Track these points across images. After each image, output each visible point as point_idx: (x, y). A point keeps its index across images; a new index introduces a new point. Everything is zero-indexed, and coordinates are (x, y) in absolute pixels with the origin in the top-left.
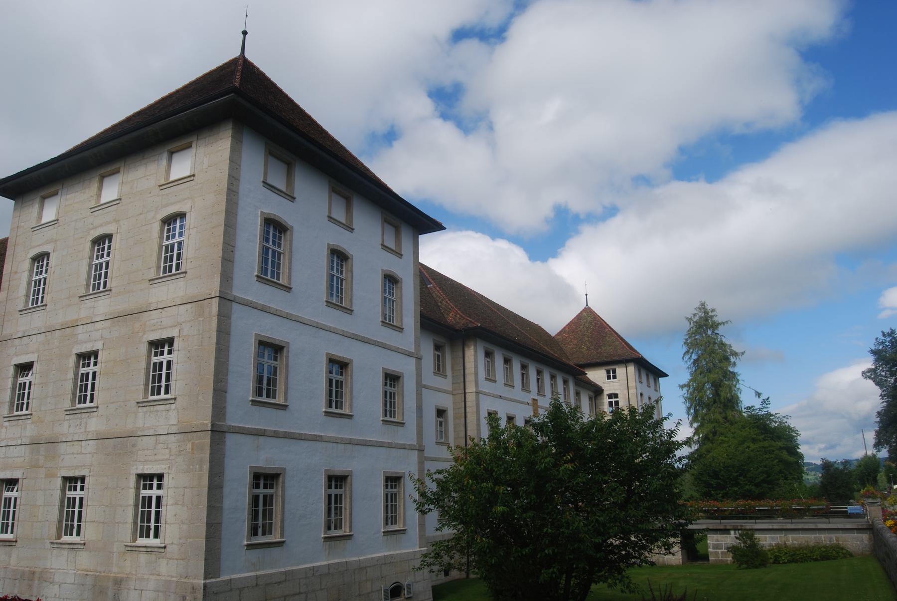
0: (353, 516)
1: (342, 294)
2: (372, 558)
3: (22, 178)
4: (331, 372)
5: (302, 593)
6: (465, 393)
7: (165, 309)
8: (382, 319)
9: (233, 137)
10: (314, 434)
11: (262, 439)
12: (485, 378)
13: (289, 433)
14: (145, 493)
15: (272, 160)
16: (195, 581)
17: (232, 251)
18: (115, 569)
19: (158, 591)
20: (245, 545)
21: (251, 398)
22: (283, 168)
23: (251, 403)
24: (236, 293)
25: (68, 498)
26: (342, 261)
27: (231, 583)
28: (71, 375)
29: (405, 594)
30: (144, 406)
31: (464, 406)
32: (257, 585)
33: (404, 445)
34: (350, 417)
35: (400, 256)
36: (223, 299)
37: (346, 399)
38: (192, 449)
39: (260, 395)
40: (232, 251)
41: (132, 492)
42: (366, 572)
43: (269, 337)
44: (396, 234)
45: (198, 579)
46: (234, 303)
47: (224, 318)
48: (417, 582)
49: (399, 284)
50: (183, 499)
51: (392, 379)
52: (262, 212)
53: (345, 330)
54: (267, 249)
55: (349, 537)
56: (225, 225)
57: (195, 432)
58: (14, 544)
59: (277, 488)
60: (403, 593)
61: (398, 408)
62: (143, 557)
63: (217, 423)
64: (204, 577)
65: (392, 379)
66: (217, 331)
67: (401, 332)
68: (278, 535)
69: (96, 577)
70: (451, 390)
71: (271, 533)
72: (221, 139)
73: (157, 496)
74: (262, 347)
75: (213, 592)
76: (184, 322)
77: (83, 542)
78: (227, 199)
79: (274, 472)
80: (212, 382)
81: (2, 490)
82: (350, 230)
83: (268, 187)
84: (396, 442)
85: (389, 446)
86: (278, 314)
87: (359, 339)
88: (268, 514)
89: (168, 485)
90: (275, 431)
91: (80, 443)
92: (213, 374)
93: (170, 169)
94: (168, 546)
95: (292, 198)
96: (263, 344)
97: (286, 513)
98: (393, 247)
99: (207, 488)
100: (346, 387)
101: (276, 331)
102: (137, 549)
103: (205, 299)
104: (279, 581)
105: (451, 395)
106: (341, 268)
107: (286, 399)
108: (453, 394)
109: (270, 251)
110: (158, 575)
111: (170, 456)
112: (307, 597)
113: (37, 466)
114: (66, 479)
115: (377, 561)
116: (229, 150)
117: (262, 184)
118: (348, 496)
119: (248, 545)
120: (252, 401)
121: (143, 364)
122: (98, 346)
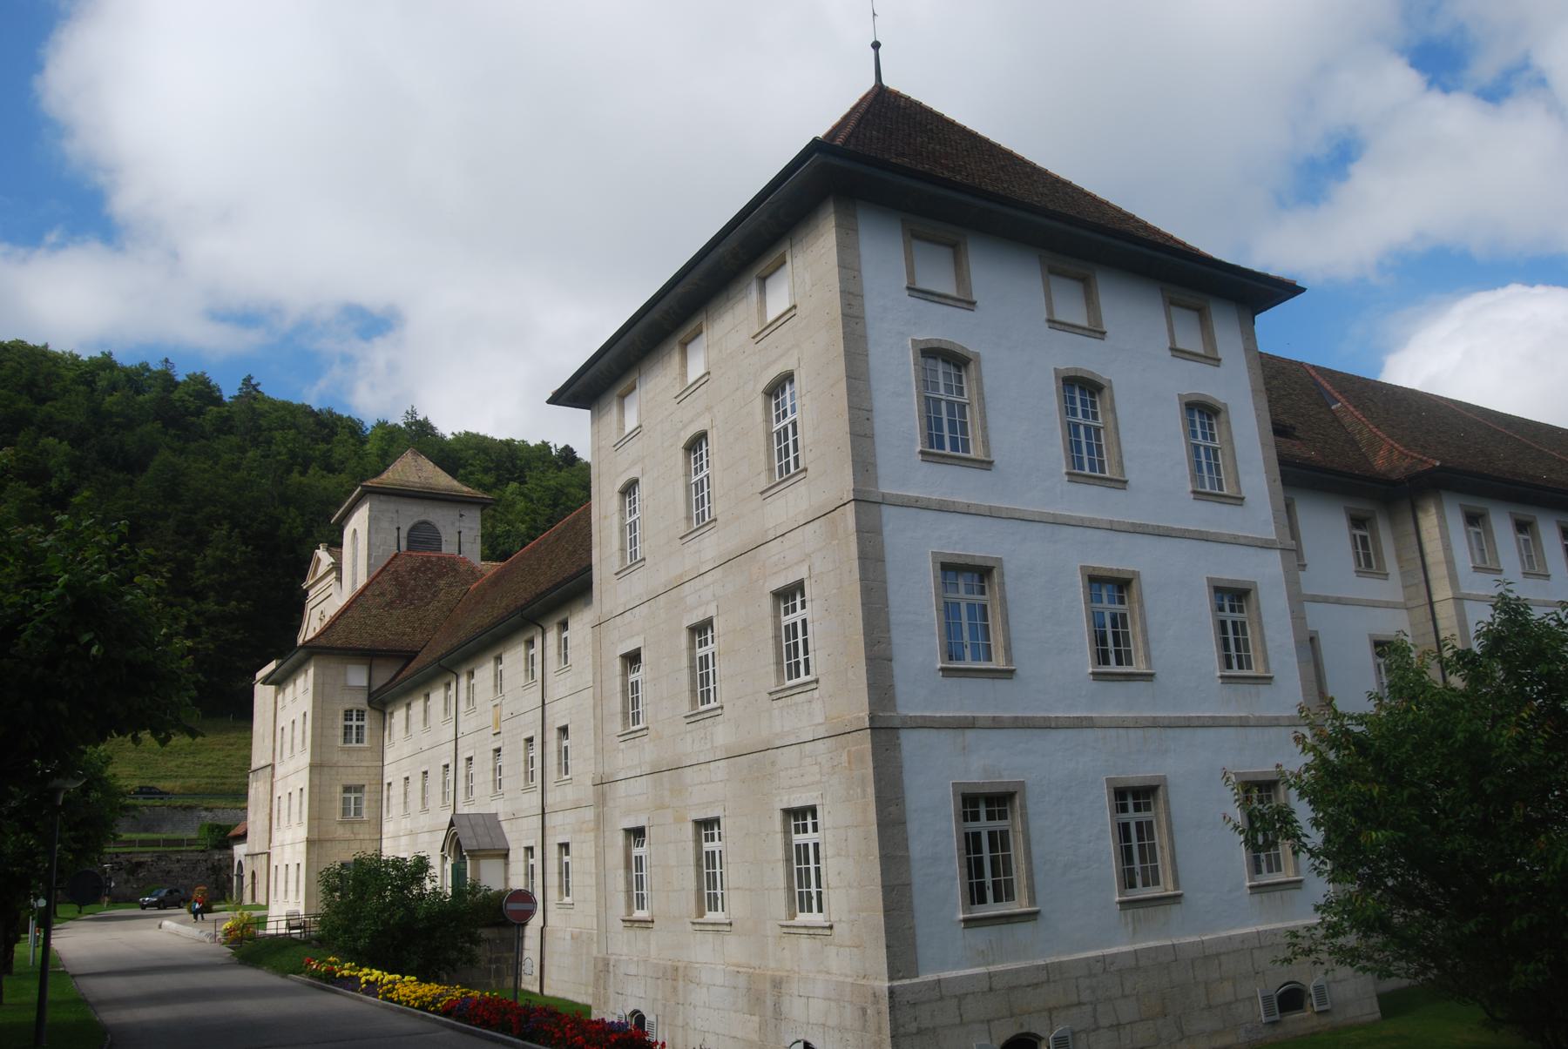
0: (1178, 860)
1: (1218, 473)
2: (1230, 938)
3: (576, 385)
4: (1221, 609)
5: (1084, 1004)
6: (1431, 604)
7: (786, 535)
8: (1067, 467)
9: (838, 226)
10: (1075, 715)
11: (970, 734)
12: (1474, 567)
13: (1023, 718)
14: (799, 839)
15: (920, 248)
16: (877, 984)
17: (868, 419)
18: (772, 965)
19: (829, 999)
20: (961, 921)
21: (939, 665)
22: (1192, 318)
23: (941, 673)
24: (886, 487)
25: (796, 845)
26: (1209, 418)
27: (940, 987)
28: (685, 662)
29: (1312, 1005)
30: (779, 698)
31: (1432, 629)
32: (991, 989)
33: (1277, 718)
34: (1148, 677)
35: (1216, 363)
36: (863, 503)
37: (1136, 645)
38: (849, 763)
39: (1106, 662)
40: (868, 419)
41: (779, 838)
42: (1220, 965)
43: (959, 556)
44: (956, 270)
45: (880, 980)
46: (883, 507)
47: (869, 535)
48: (1340, 981)
49: (1222, 416)
50: (847, 846)
51: (1232, 596)
52: (913, 341)
53: (1116, 519)
54: (1197, 447)
55: (1176, 899)
56: (848, 377)
57: (849, 733)
58: (651, 925)
59: (1013, 819)
60: (1309, 1002)
61: (1255, 650)
62: (805, 943)
63: (881, 714)
64: (889, 977)
65: (1232, 596)
66: (859, 558)
67: (1241, 505)
68: (1025, 901)
69: (750, 976)
70: (1402, 600)
71: (1279, 869)
72: (822, 235)
73: (814, 844)
74: (1096, 586)
75: (908, 1002)
76: (813, 553)
77: (727, 921)
78: (844, 333)
79: (1002, 789)
80: (862, 645)
81: (631, 845)
82: (1098, 335)
83: (920, 295)
84: (1257, 715)
85: (1243, 723)
86: (973, 511)
87: (1146, 530)
88: (1148, 853)
89: (824, 825)
90: (994, 717)
91: (707, 765)
92: (862, 631)
93: (765, 306)
94: (835, 926)
95: (970, 304)
96: (951, 569)
97: (1035, 861)
98: (1200, 349)
99: (876, 826)
100: (1134, 623)
101: (971, 541)
102: (795, 930)
103: (836, 509)
104: (1035, 981)
105: (1405, 611)
106: (1210, 430)
107: (1009, 659)
108: (1407, 609)
109: (1082, 429)
110: (828, 973)
111: (821, 775)
112: (1095, 1010)
113: (662, 807)
114: (628, 831)
115: (1243, 941)
116: (835, 249)
117: (907, 293)
118: (1164, 824)
119: (966, 921)
120: (942, 669)
121: (769, 632)
122: (711, 611)
